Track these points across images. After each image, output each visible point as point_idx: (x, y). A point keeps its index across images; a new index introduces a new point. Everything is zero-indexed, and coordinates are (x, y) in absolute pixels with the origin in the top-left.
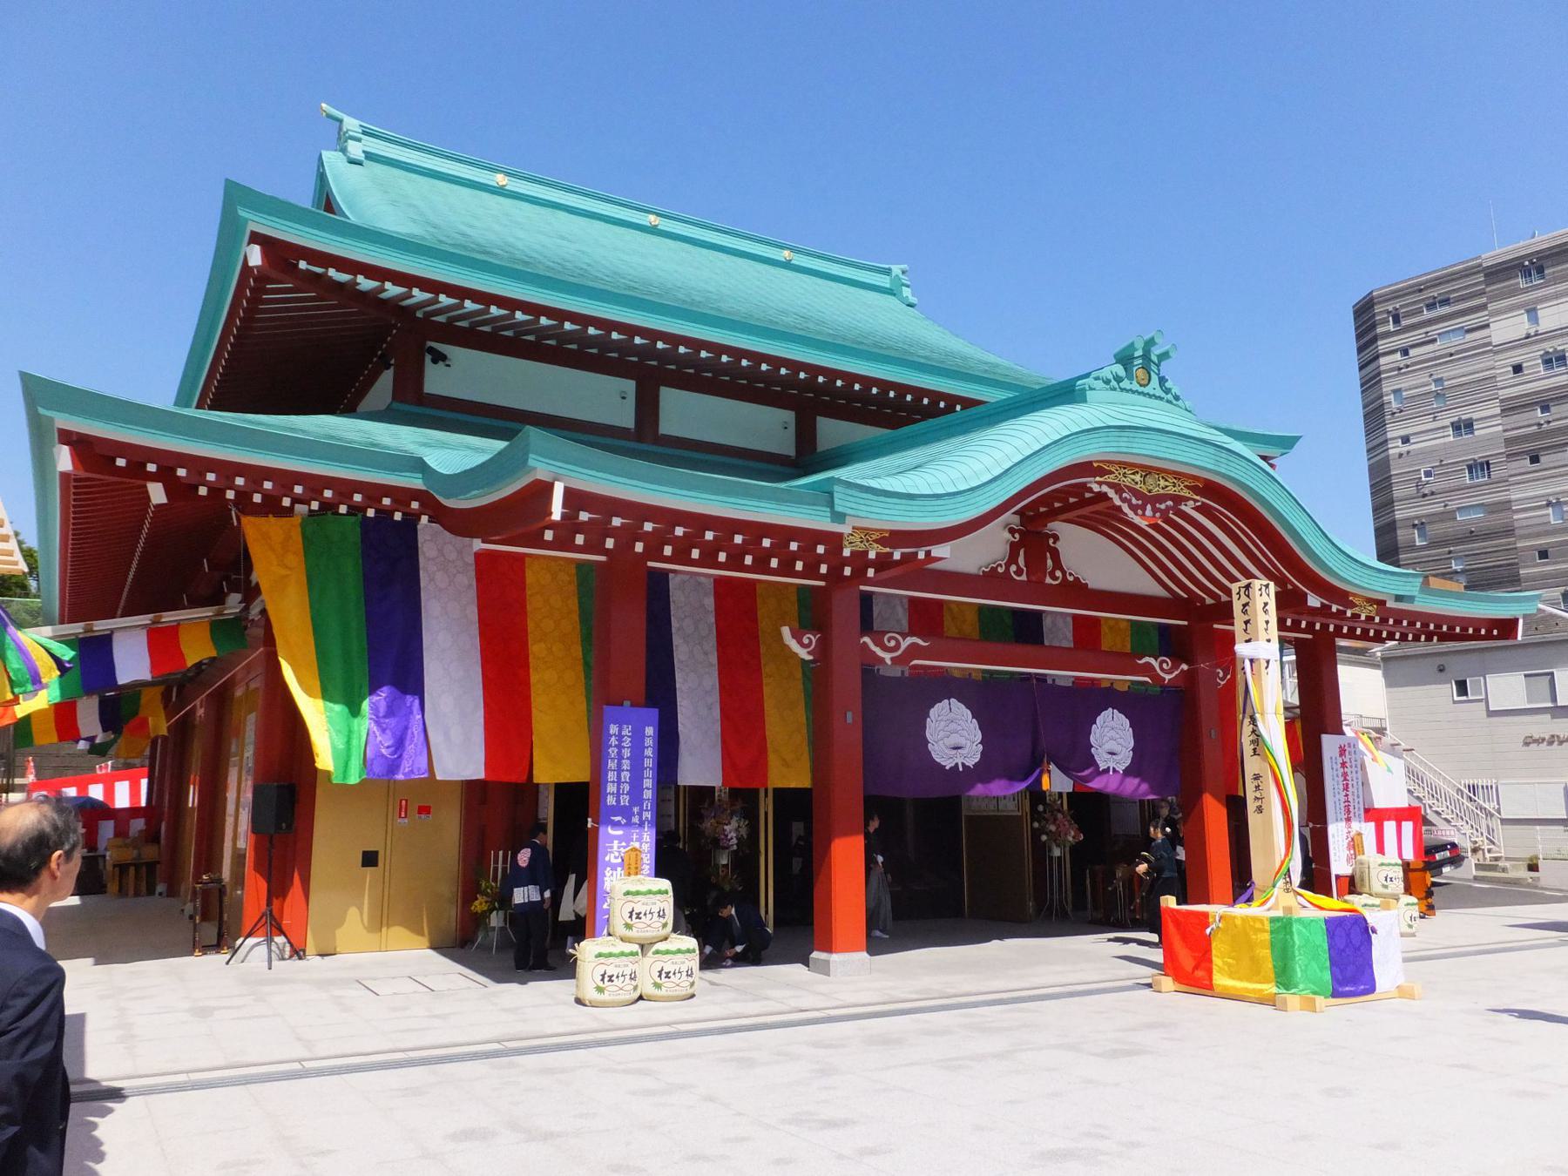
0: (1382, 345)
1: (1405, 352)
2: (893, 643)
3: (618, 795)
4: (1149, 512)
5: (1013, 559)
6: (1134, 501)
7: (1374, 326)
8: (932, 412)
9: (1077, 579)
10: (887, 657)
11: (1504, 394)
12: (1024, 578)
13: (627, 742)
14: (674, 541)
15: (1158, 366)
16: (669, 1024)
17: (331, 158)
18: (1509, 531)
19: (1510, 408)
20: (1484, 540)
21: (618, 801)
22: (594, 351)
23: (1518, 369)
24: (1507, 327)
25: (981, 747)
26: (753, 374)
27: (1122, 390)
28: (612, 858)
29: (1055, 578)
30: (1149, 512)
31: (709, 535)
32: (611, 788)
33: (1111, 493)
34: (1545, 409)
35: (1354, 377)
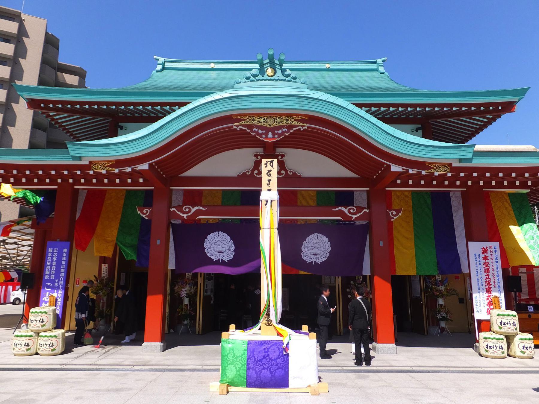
2: (187, 210)
3: (50, 275)
6: (260, 131)
13: (55, 255)
14: (460, 179)
16: (480, 367)
21: (50, 277)
25: (234, 253)
27: (258, 80)
28: (45, 299)
32: (47, 272)
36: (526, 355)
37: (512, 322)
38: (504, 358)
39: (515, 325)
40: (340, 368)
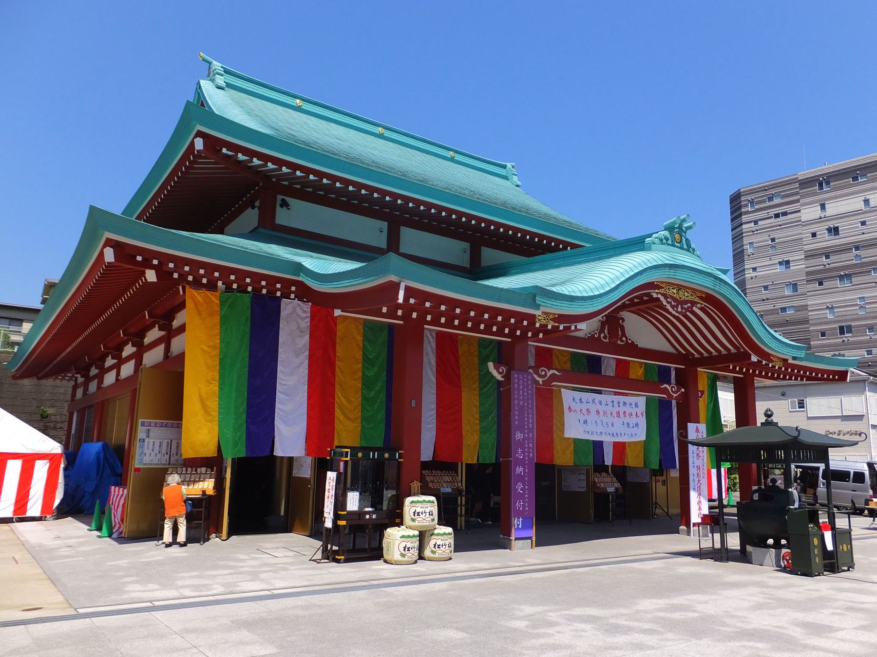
0: (744, 218)
1: (756, 222)
4: (679, 310)
5: (602, 330)
7: (740, 208)
8: (556, 249)
9: (633, 342)
10: (540, 380)
11: (806, 248)
12: (607, 340)
14: (510, 326)
15: (685, 233)
16: (350, 582)
17: (205, 84)
18: (806, 321)
19: (810, 255)
20: (793, 325)
22: (322, 193)
23: (814, 235)
24: (809, 213)
26: (426, 214)
29: (622, 341)
30: (679, 310)
31: (513, 321)
33: (662, 299)
34: (827, 257)
35: (728, 235)
36: (406, 559)
37: (428, 510)
38: (416, 562)
39: (432, 515)
40: (149, 604)
